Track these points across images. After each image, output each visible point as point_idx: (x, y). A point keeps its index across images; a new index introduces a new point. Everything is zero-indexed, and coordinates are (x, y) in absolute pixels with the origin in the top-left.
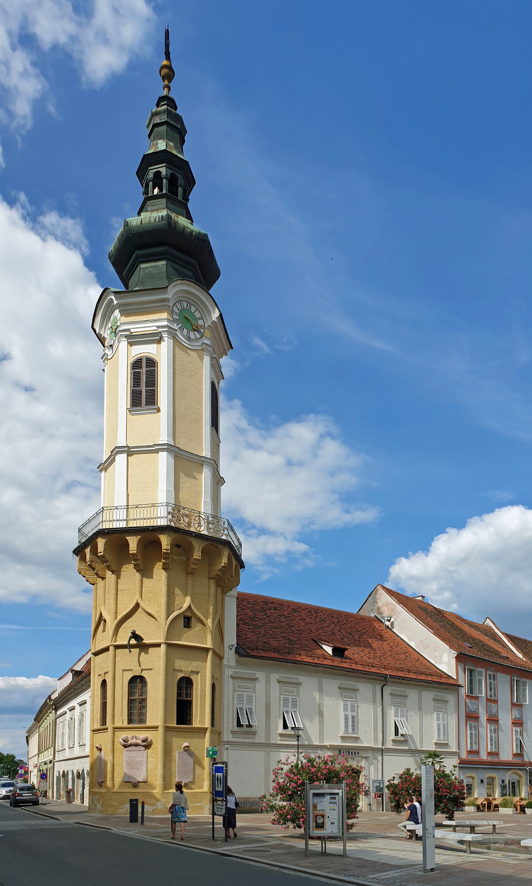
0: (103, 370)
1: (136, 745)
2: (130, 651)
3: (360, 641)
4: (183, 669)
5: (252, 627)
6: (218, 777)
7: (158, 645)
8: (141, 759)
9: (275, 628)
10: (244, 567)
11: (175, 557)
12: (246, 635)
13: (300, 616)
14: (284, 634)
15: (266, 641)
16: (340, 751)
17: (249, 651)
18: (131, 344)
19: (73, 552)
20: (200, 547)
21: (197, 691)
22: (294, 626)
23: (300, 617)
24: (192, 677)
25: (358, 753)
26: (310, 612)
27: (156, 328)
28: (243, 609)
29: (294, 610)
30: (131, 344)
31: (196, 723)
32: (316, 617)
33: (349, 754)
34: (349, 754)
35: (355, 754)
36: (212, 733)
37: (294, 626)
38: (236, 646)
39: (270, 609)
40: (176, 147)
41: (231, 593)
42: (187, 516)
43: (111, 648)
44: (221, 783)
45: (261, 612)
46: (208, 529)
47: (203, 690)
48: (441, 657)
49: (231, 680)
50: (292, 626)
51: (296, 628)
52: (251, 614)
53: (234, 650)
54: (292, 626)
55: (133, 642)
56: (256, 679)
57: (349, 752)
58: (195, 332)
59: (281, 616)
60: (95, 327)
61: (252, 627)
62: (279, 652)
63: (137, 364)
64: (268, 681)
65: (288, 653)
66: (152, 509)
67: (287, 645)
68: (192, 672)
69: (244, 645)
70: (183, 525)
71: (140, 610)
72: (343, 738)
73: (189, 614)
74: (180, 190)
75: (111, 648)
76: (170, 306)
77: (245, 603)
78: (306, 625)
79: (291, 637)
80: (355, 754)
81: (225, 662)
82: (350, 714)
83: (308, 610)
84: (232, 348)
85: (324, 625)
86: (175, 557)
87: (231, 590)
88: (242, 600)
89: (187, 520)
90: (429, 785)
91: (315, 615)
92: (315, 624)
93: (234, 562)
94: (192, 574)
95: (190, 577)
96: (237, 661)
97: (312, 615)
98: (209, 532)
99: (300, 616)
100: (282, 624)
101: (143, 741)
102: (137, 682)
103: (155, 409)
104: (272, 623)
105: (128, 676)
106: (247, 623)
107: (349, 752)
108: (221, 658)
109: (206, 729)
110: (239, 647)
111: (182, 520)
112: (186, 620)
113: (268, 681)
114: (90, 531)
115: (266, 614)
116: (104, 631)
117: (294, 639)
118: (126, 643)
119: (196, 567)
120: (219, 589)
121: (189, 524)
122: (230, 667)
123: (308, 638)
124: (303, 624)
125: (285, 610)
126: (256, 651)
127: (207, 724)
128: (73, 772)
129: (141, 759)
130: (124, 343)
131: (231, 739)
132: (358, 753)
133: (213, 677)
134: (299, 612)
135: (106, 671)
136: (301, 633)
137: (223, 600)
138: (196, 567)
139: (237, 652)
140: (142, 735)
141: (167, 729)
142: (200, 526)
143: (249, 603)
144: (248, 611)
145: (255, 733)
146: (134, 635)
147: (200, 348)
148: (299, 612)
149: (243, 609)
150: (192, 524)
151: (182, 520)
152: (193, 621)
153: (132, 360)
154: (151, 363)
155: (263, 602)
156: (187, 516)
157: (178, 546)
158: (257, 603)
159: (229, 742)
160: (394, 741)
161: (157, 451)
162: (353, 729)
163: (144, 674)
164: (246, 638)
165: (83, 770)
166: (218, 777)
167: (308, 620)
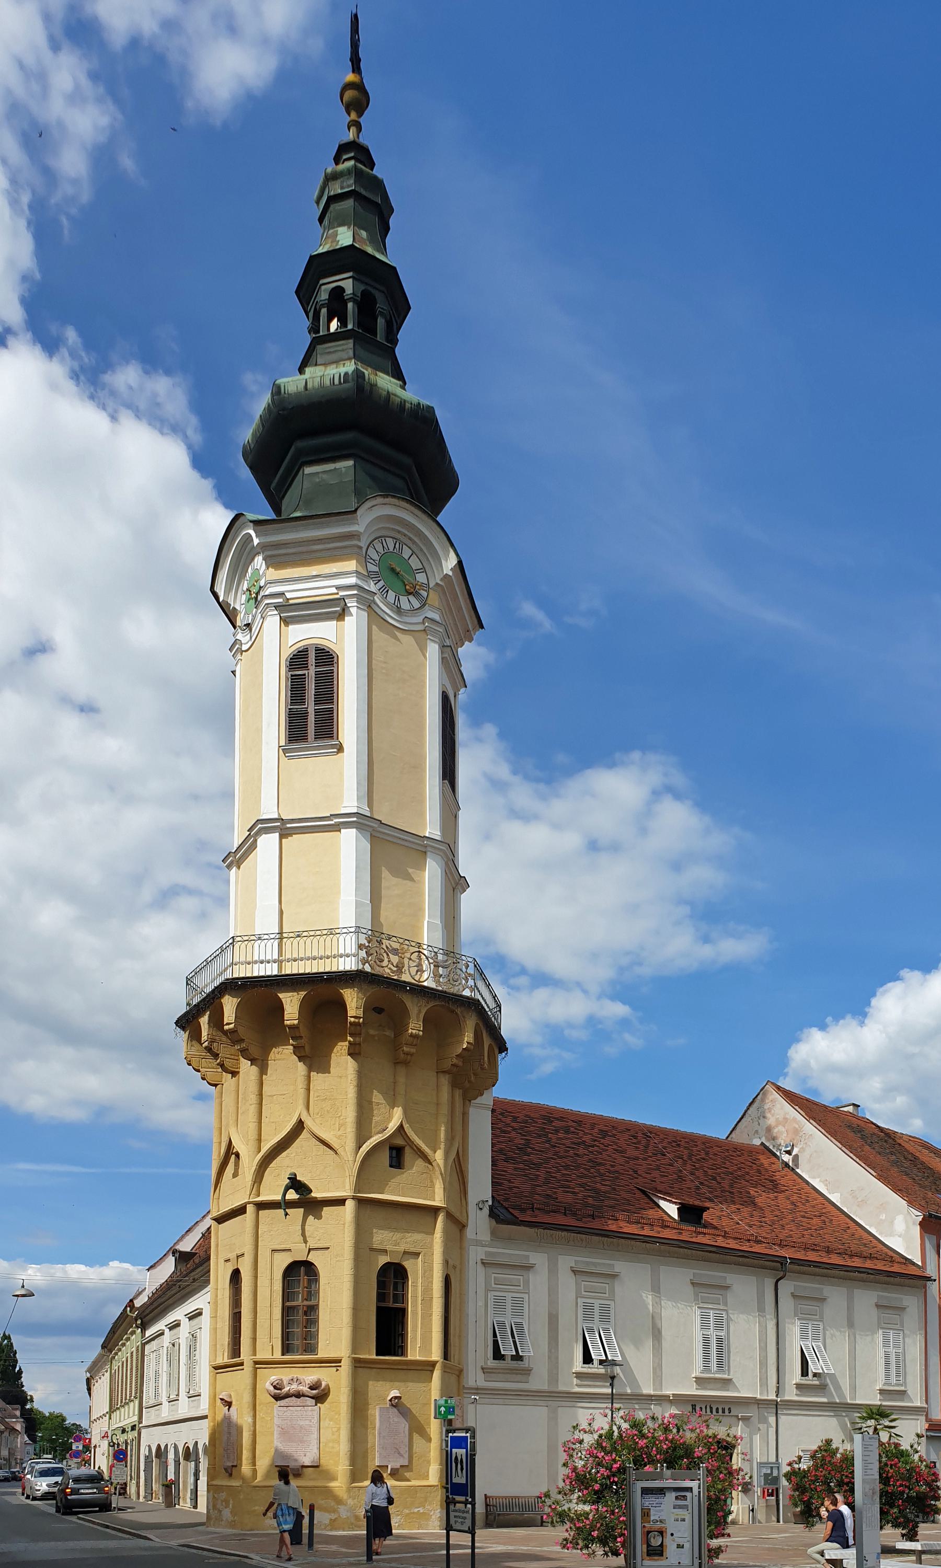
0: (234, 672)
1: (298, 1395)
2: (286, 1214)
3: (732, 1193)
4: (389, 1247)
5: (521, 1166)
6: (456, 1457)
7: (341, 1202)
8: (307, 1422)
9: (567, 1167)
10: (507, 1050)
11: (372, 1032)
12: (509, 1181)
13: (616, 1144)
14: (584, 1180)
15: (549, 1192)
16: (694, 1407)
17: (516, 1213)
18: (286, 621)
19: (177, 1023)
20: (420, 1011)
21: (415, 1291)
22: (604, 1165)
23: (615, 1147)
24: (407, 1264)
25: (729, 1409)
26: (635, 1137)
27: (334, 590)
28: (505, 1132)
29: (604, 1134)
30: (286, 621)
31: (414, 1353)
32: (647, 1147)
33: (711, 1412)
34: (711, 1412)
35: (723, 1412)
36: (445, 1371)
37: (604, 1165)
38: (490, 1203)
39: (557, 1131)
40: (372, 240)
41: (479, 1100)
42: (395, 952)
43: (250, 1209)
44: (462, 1469)
45: (540, 1136)
46: (437, 976)
47: (428, 1290)
48: (892, 1222)
49: (480, 1268)
50: (600, 1164)
51: (608, 1167)
52: (519, 1141)
53: (486, 1211)
54: (600, 1164)
55: (292, 1195)
56: (529, 1268)
57: (711, 1408)
58: (411, 598)
59: (578, 1144)
60: (217, 589)
61: (521, 1166)
62: (574, 1214)
63: (298, 660)
64: (553, 1271)
65: (593, 1216)
66: (329, 938)
67: (590, 1200)
68: (405, 1253)
69: (506, 1200)
70: (387, 970)
71: (305, 1134)
72: (699, 1380)
73: (399, 1142)
74: (381, 322)
75: (250, 1209)
76: (361, 548)
77: (508, 1120)
78: (628, 1163)
79: (598, 1186)
80: (723, 1412)
81: (470, 1233)
82: (713, 1334)
83: (632, 1133)
84: (482, 627)
85: (663, 1162)
86: (372, 1032)
87: (482, 1095)
88: (502, 1114)
89: (395, 959)
90: (869, 1472)
91: (644, 1142)
92: (645, 1159)
93: (487, 1041)
94: (406, 1063)
95: (402, 1070)
96: (493, 1233)
97: (639, 1142)
98: (438, 982)
99: (616, 1144)
100: (580, 1160)
101: (311, 1388)
102: (300, 1274)
103: (333, 746)
104: (561, 1157)
105: (283, 1261)
106: (512, 1158)
107: (711, 1408)
108: (462, 1227)
109: (433, 1364)
110: (497, 1204)
111: (386, 960)
112: (394, 1152)
113: (553, 1271)
114: (208, 983)
115: (548, 1141)
116: (235, 1175)
117: (603, 1188)
118: (278, 1197)
119: (413, 1050)
120: (458, 1093)
121: (400, 968)
122: (478, 1243)
123: (632, 1187)
124: (621, 1160)
125: (586, 1134)
126: (529, 1212)
127: (436, 1354)
128: (176, 1447)
129: (307, 1422)
130: (273, 620)
131: (481, 1382)
132: (729, 1409)
133: (446, 1263)
134: (614, 1136)
135: (239, 1253)
136: (617, 1178)
137: (465, 1115)
138: (413, 1050)
139: (493, 1214)
140: (310, 1376)
141: (358, 1364)
142: (420, 970)
143: (515, 1119)
144: (513, 1134)
145: (527, 1372)
146: (295, 1183)
147: (421, 627)
148: (614, 1136)
149: (505, 1132)
150: (406, 968)
151: (386, 960)
152: (408, 1154)
153: (288, 652)
154: (326, 657)
155: (544, 1117)
156: (395, 952)
157: (379, 1010)
158: (532, 1118)
159: (477, 1389)
160: (799, 1386)
161: (337, 828)
162: (720, 1364)
163: (312, 1258)
164: (510, 1188)
165: (196, 1443)
166: (456, 1457)
167: (631, 1152)
